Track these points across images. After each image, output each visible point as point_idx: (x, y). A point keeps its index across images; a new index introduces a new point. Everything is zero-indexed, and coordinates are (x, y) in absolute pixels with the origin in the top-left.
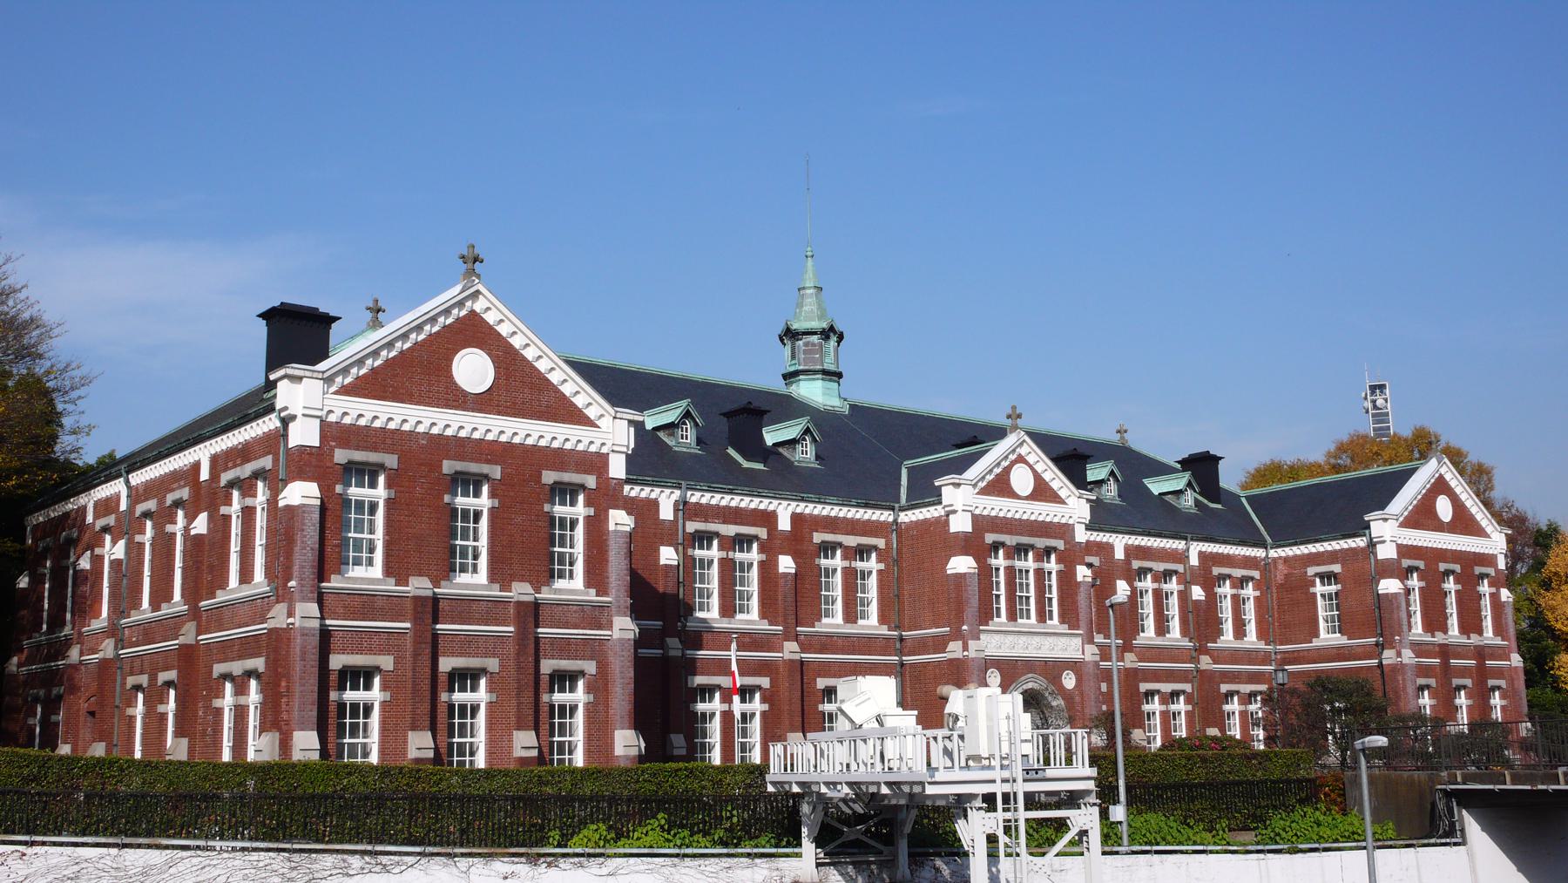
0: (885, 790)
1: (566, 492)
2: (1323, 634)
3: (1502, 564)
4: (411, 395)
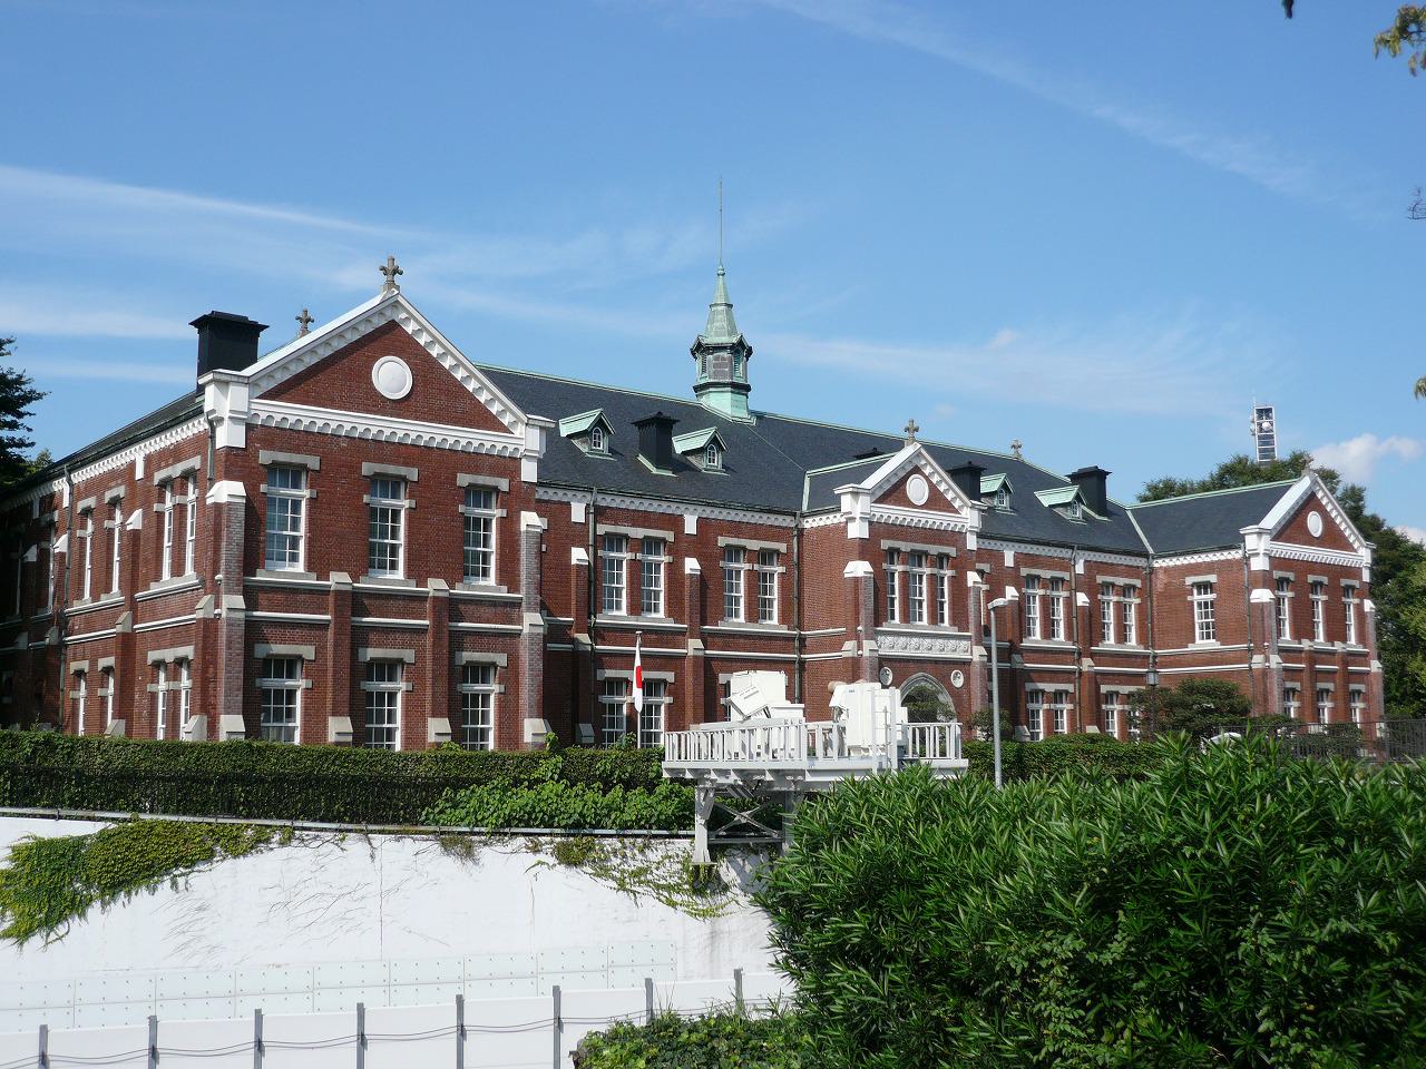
0: (769, 778)
1: (482, 495)
2: (1198, 641)
3: (1366, 576)
4: (333, 401)
